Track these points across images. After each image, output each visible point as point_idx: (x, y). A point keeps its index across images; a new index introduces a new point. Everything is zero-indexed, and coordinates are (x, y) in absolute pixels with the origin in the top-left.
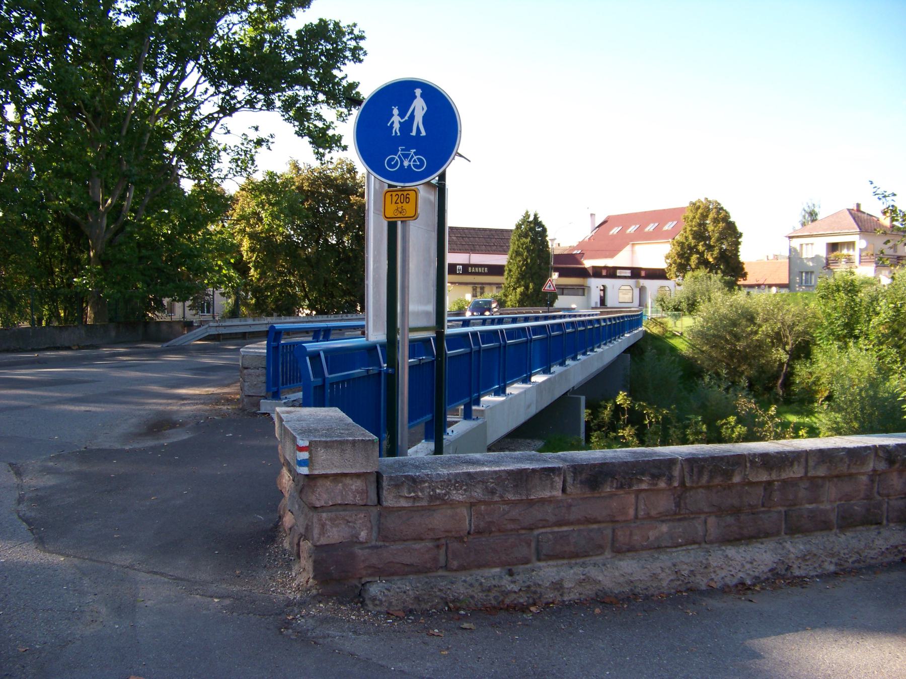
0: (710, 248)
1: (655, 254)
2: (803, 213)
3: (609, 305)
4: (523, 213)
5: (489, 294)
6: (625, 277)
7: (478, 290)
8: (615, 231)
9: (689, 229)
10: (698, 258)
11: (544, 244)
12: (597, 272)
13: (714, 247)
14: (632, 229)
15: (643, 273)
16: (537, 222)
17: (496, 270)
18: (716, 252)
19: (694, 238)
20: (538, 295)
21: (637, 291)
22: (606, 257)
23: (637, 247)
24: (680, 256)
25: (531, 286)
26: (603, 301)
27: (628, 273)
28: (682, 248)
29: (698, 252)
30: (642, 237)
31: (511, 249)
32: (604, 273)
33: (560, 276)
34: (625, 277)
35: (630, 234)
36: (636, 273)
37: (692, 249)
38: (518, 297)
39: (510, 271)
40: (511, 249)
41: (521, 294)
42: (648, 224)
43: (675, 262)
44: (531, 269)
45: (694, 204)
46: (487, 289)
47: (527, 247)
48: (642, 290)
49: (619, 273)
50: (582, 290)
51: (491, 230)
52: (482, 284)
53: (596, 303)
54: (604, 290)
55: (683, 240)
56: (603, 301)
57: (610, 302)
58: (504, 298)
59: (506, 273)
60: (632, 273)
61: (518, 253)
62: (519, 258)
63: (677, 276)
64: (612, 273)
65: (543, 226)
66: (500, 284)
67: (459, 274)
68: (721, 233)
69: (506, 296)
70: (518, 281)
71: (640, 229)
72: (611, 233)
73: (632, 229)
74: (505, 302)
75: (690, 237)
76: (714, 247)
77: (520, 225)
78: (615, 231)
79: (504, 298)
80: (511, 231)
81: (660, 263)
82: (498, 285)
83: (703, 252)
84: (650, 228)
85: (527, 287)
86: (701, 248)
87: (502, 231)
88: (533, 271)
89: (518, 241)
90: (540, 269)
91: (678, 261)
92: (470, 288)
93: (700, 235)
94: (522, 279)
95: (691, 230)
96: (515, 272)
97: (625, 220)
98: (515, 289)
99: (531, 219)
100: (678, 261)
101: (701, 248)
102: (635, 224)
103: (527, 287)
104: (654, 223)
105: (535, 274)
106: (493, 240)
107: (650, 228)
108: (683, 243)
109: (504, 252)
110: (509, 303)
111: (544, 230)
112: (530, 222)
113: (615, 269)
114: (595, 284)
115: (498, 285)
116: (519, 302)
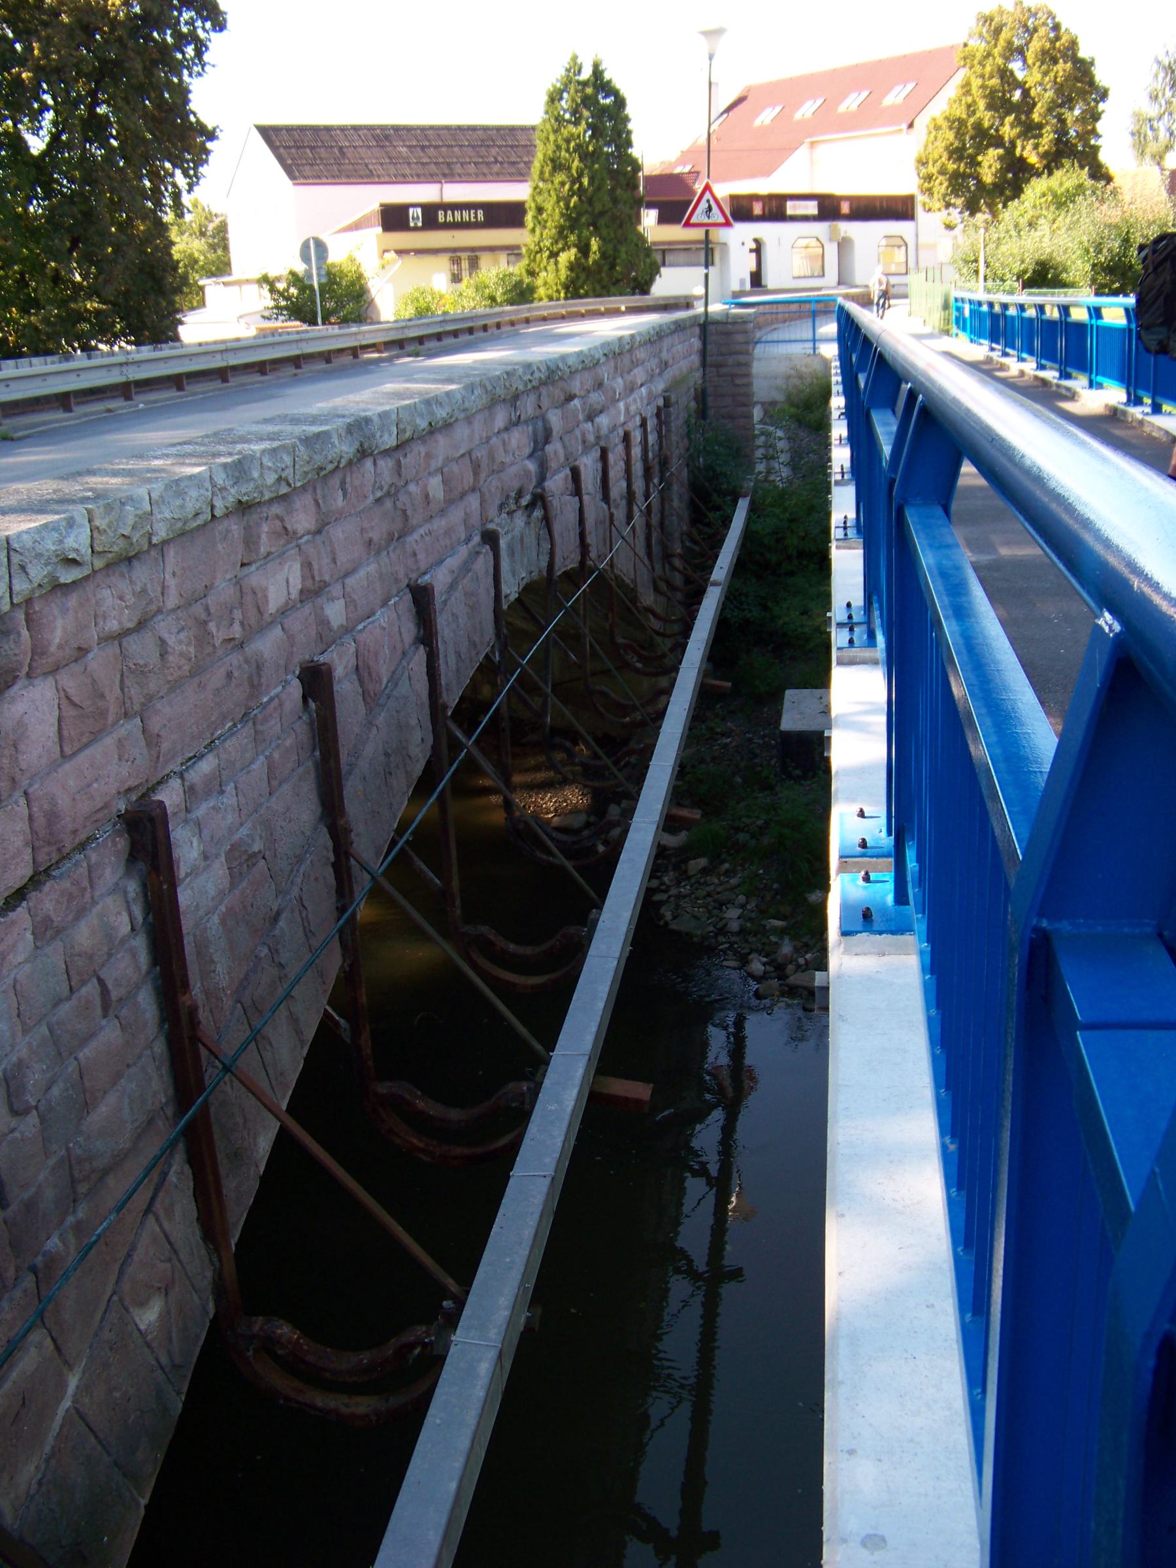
0: (1030, 130)
1: (886, 162)
2: (1155, 66)
3: (770, 286)
4: (565, 62)
5: (493, 271)
6: (805, 218)
7: (465, 265)
8: (766, 117)
9: (976, 83)
10: (1000, 158)
11: (622, 139)
12: (741, 210)
13: (1040, 126)
14: (807, 110)
15: (845, 208)
16: (600, 83)
17: (506, 215)
18: (1047, 138)
19: (989, 107)
20: (612, 267)
21: (832, 251)
22: (753, 175)
23: (820, 149)
24: (957, 153)
25: (595, 244)
26: (757, 279)
27: (811, 208)
28: (959, 134)
29: (998, 142)
30: (831, 123)
31: (540, 156)
32: (757, 209)
33: (662, 220)
34: (805, 218)
35: (803, 122)
36: (828, 209)
37: (985, 138)
38: (564, 273)
39: (540, 210)
40: (540, 156)
41: (571, 267)
42: (843, 96)
43: (942, 172)
44: (590, 201)
45: (987, 19)
46: (485, 260)
47: (579, 147)
48: (844, 246)
49: (791, 208)
50: (707, 253)
51: (486, 129)
52: (473, 249)
53: (742, 282)
54: (758, 250)
55: (961, 112)
56: (757, 279)
57: (771, 279)
58: (527, 280)
59: (529, 218)
60: (821, 207)
61: (557, 165)
62: (560, 177)
63: (948, 205)
64: (775, 209)
65: (616, 93)
66: (518, 247)
67: (416, 229)
68: (1059, 89)
69: (532, 273)
70: (561, 234)
71: (828, 107)
72: (757, 123)
73: (807, 110)
74: (532, 289)
75: (982, 104)
76: (1040, 126)
77: (561, 92)
78: (766, 117)
79: (527, 280)
80: (533, 128)
81: (900, 181)
82: (513, 251)
83: (1013, 144)
84: (851, 103)
85: (584, 250)
86: (1008, 131)
87: (512, 130)
88: (598, 207)
89: (556, 131)
90: (615, 201)
91: (951, 166)
92: (443, 261)
93: (1005, 98)
94: (572, 229)
95: (983, 87)
96: (554, 214)
97: (789, 91)
98: (554, 255)
99: (586, 74)
100: (951, 166)
101: (1008, 131)
102: (814, 97)
103: (584, 250)
104: (859, 90)
105: (602, 214)
106: (494, 151)
107: (851, 103)
108: (962, 122)
109: (520, 176)
110: (542, 292)
111: (620, 103)
112: (585, 84)
113: (782, 199)
114: (739, 236)
115: (513, 251)
116: (566, 287)
